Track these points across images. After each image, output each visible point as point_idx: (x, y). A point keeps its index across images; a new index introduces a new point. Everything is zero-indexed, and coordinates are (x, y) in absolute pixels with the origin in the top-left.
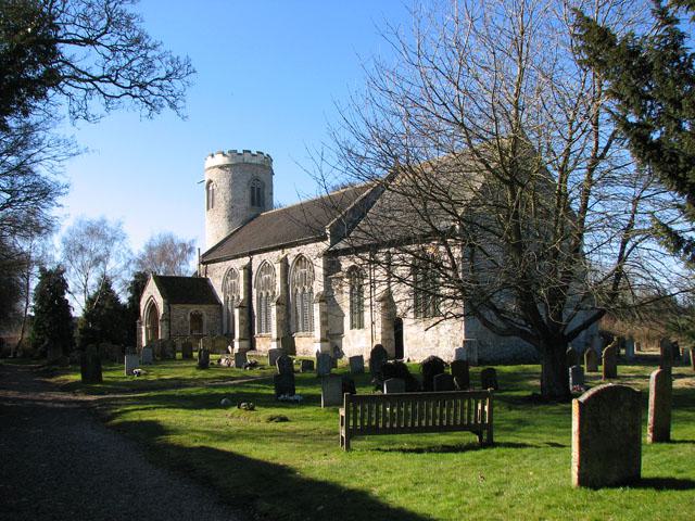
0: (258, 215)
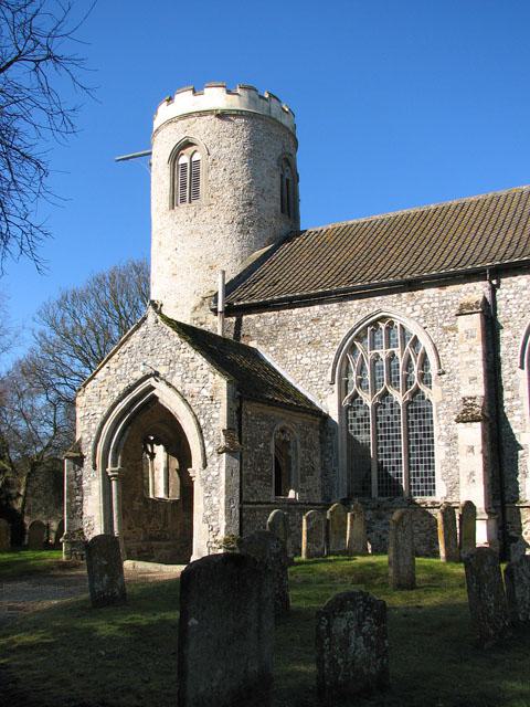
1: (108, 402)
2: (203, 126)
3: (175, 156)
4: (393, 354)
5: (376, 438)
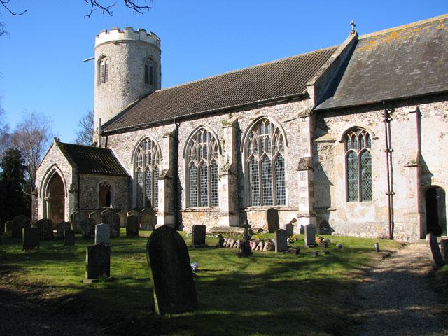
0: (150, 93)
1: (44, 174)
2: (109, 49)
3: (100, 62)
4: (268, 137)
5: (145, 185)
